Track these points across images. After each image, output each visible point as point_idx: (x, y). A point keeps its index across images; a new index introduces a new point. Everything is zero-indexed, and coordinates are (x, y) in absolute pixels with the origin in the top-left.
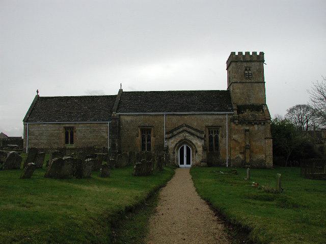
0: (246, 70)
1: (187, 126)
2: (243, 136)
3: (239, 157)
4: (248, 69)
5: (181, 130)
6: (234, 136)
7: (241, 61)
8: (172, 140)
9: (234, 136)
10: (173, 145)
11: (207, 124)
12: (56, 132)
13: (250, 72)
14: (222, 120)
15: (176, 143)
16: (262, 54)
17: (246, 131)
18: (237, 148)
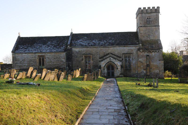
0: (148, 19)
1: (111, 54)
2: (145, 59)
3: (143, 72)
4: (149, 18)
5: (108, 56)
6: (140, 59)
7: (145, 13)
8: (102, 63)
9: (140, 59)
10: (104, 65)
11: (123, 52)
12: (33, 59)
13: (150, 20)
14: (132, 50)
15: (105, 64)
16: (158, 8)
17: (147, 56)
18: (142, 67)
